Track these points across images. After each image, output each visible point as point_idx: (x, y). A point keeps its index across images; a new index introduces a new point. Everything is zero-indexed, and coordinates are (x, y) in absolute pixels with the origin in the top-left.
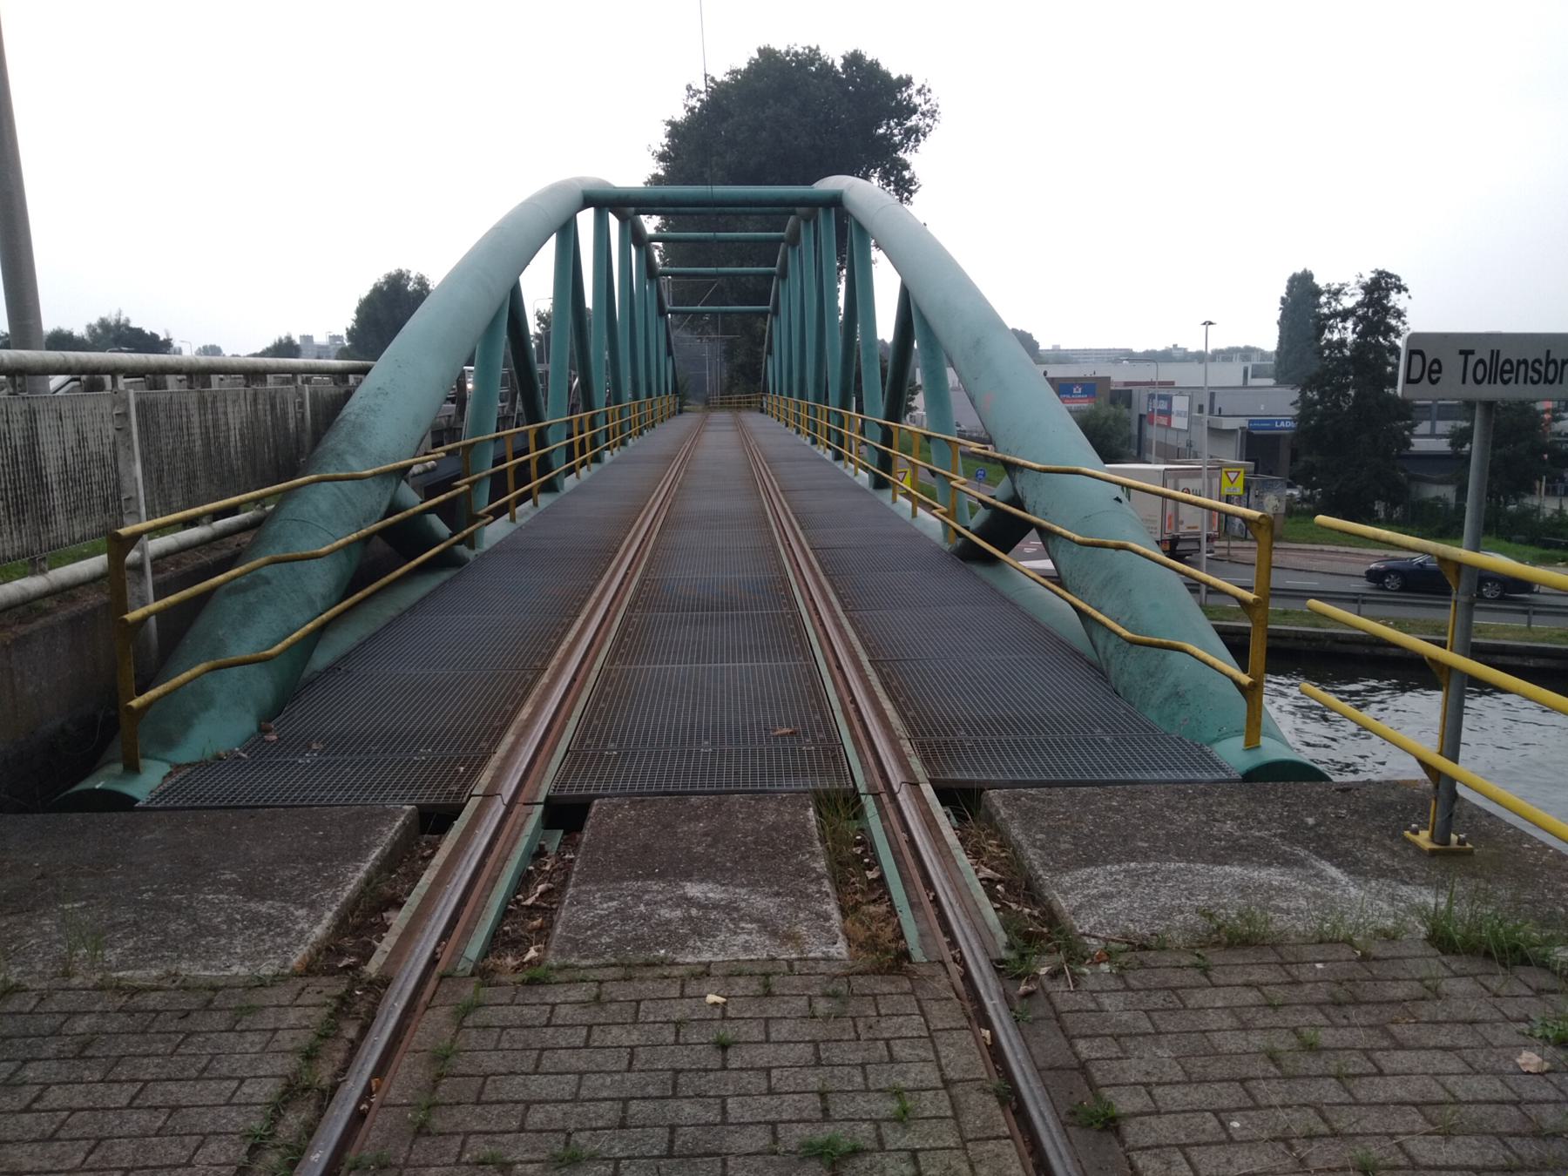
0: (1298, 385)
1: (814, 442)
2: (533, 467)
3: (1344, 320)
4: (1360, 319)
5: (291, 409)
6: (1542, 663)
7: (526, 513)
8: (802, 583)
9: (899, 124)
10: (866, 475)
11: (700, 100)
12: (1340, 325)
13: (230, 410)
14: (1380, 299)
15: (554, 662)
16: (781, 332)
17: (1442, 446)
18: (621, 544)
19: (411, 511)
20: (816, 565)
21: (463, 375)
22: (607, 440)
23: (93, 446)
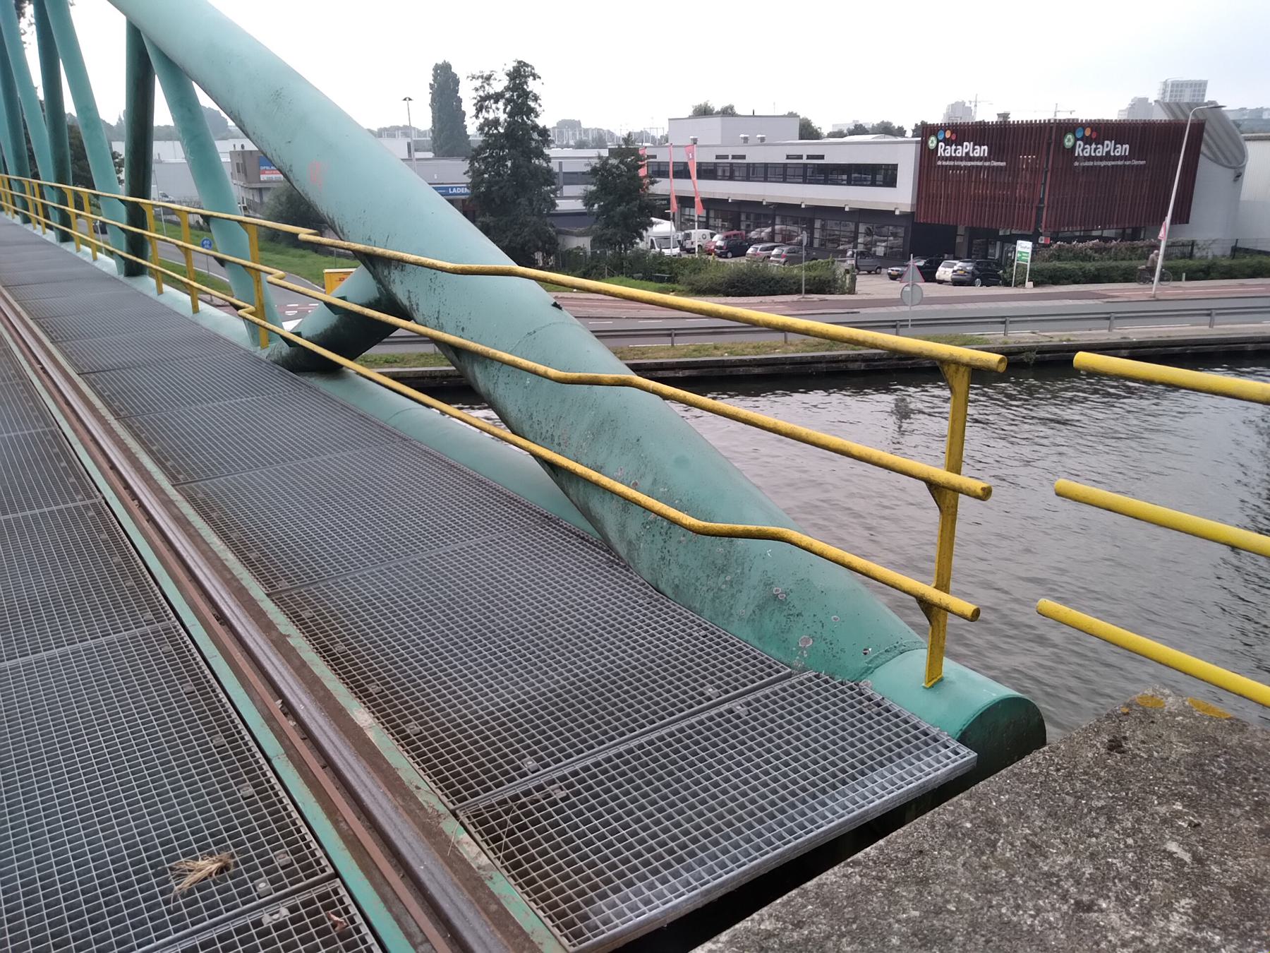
0: (467, 158)
1: (27, 220)
3: (496, 102)
4: (508, 101)
6: (687, 373)
8: (87, 438)
10: (112, 262)
12: (494, 106)
14: (522, 84)
17: (578, 206)
20: (98, 403)
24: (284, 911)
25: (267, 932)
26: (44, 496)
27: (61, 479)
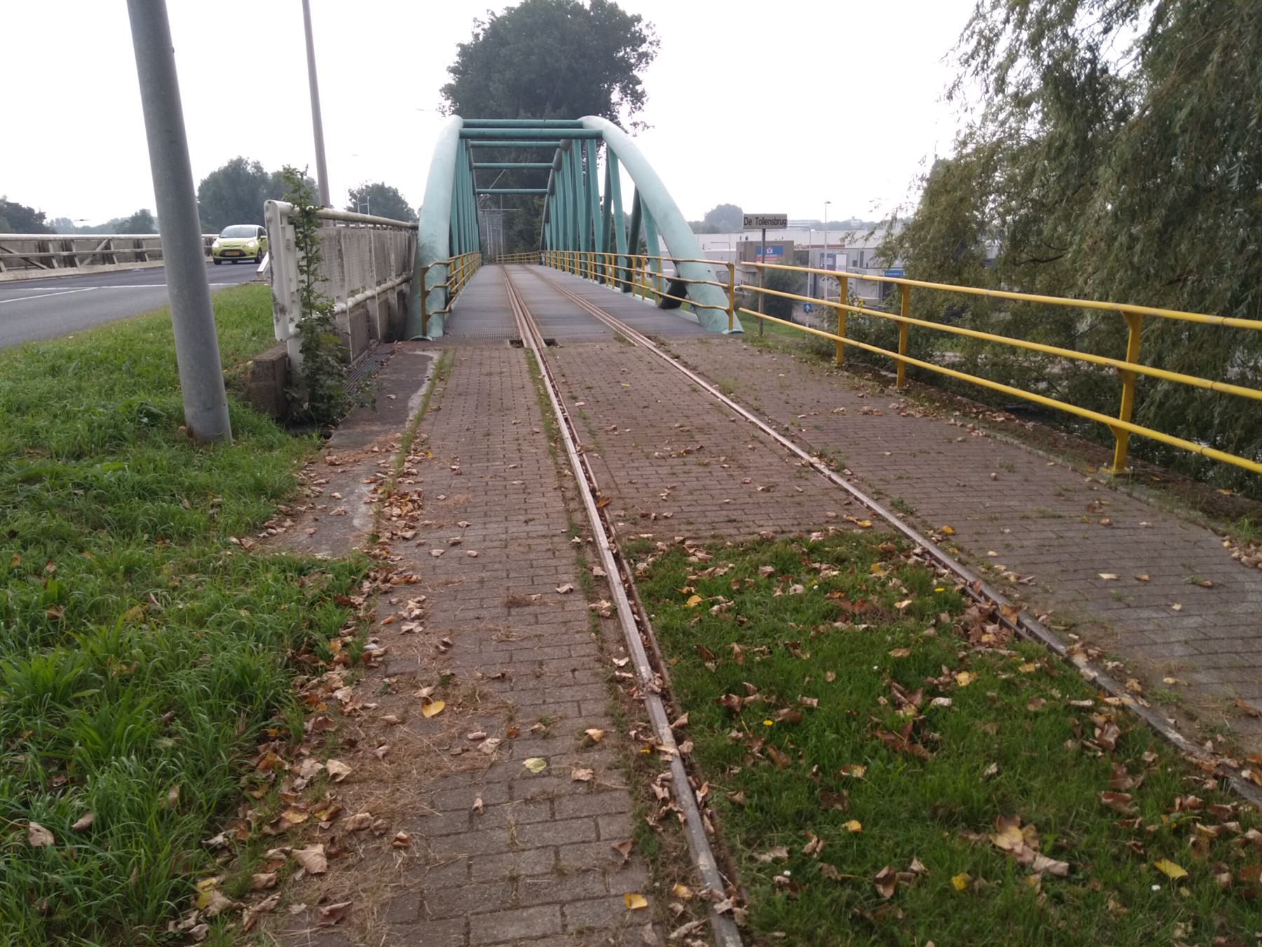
9: (633, 50)
11: (483, 29)
16: (555, 206)
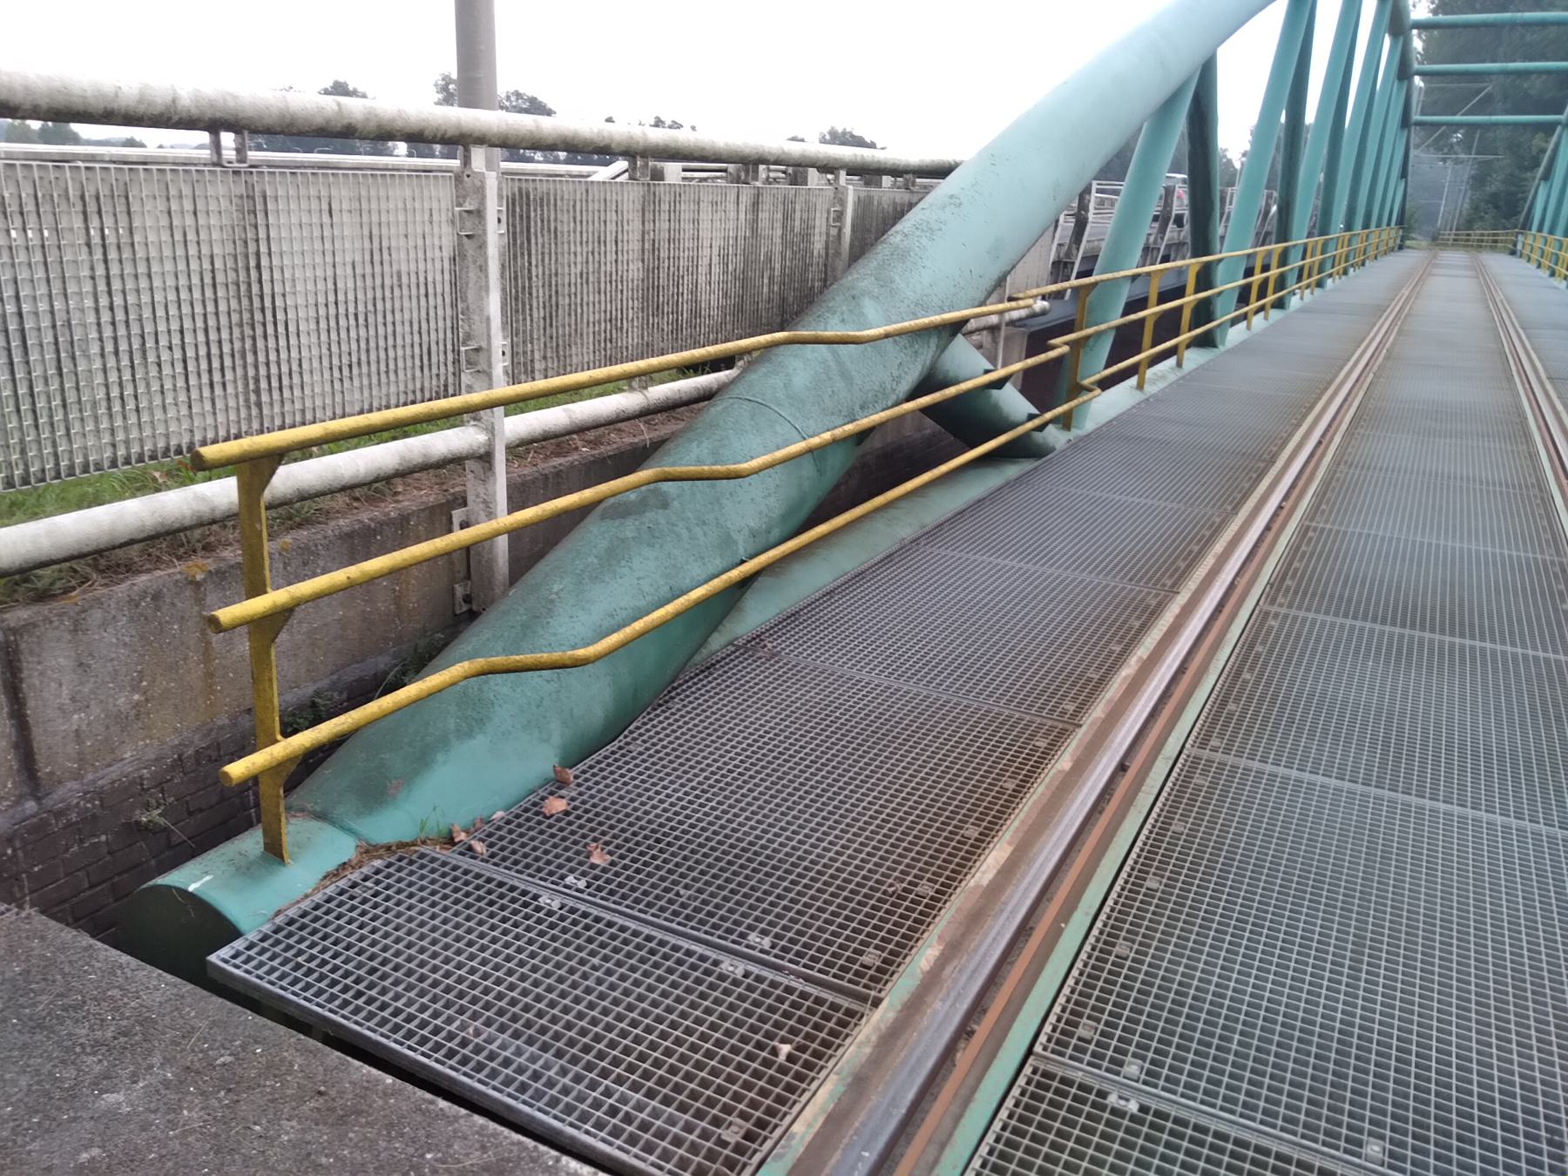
2: (1186, 315)
5: (820, 223)
7: (1163, 377)
13: (705, 216)
15: (1098, 711)
18: (1282, 447)
19: (964, 386)
21: (1087, 190)
22: (1333, 267)
23: (402, 261)
24: (1133, 1107)
25: (1103, 1108)
26: (1532, 636)
27: (1296, 592)
